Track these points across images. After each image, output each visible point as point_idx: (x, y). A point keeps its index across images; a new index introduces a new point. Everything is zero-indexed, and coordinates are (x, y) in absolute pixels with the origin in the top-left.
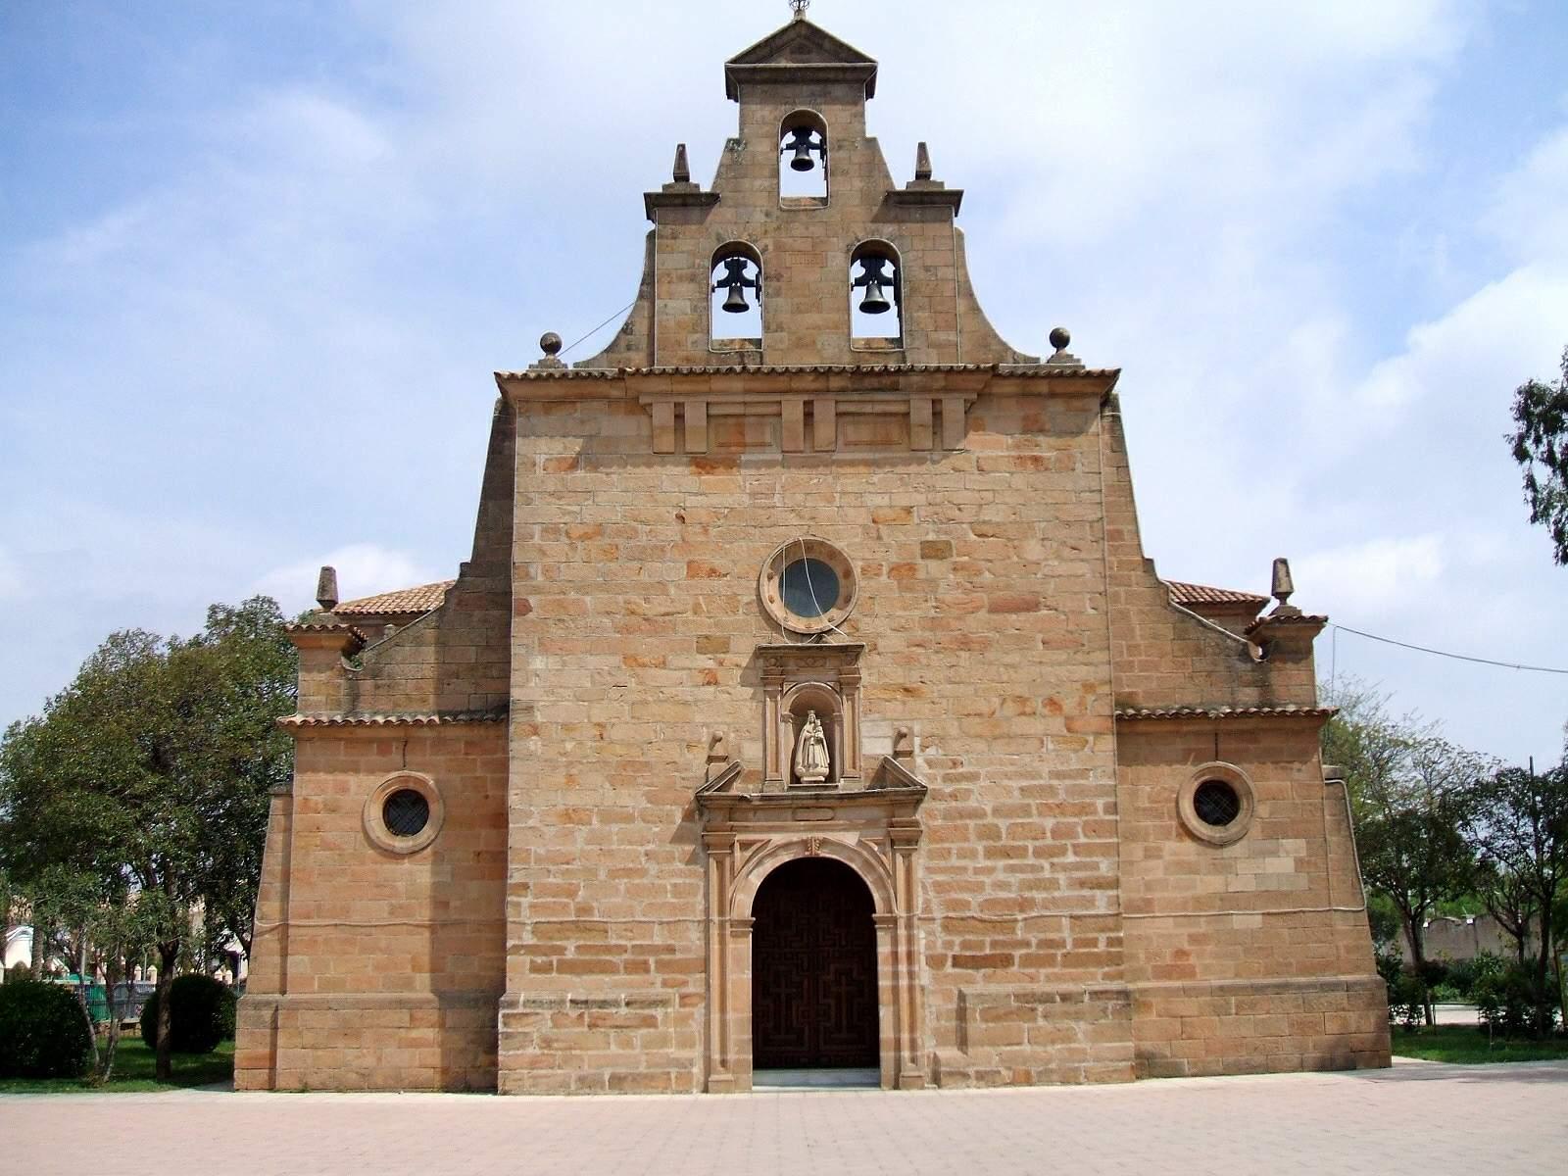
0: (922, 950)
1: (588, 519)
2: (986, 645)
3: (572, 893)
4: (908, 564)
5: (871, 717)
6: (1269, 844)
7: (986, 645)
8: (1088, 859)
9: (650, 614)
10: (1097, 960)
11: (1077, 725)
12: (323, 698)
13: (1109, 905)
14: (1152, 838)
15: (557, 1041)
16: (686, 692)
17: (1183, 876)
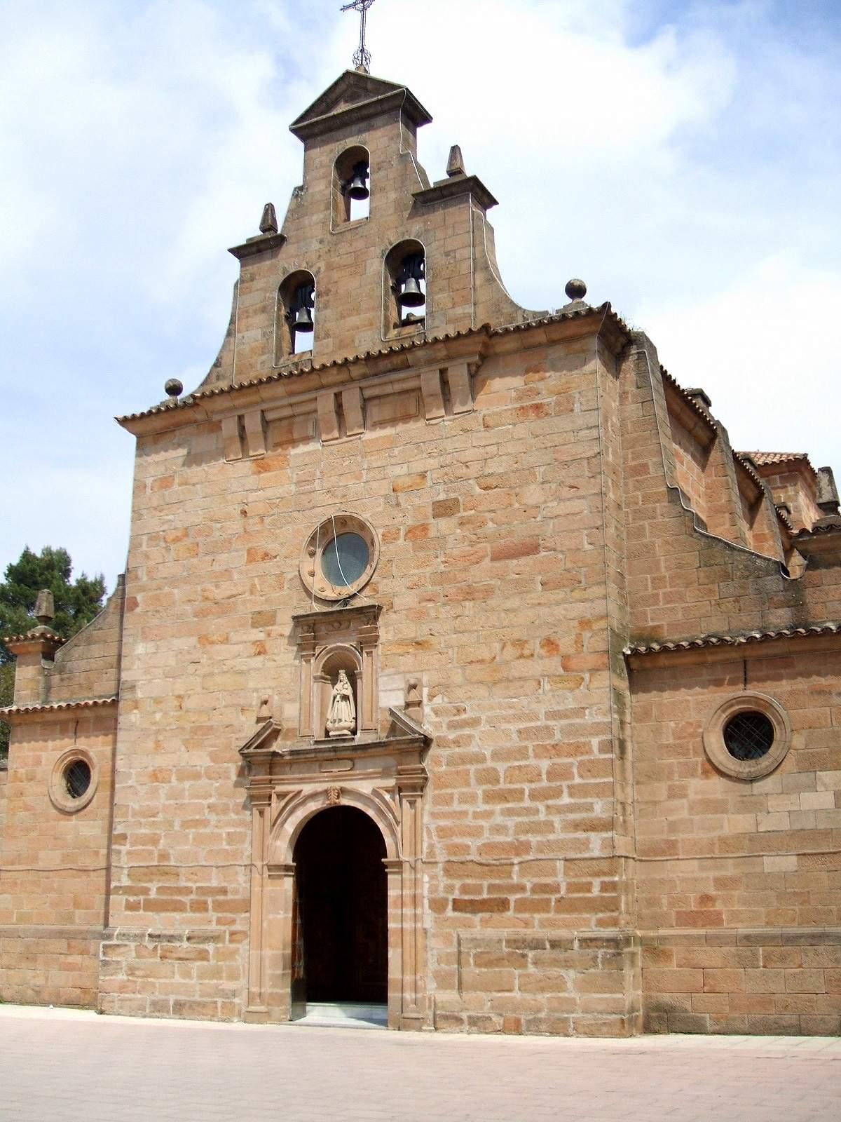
0: (426, 893)
1: (179, 525)
2: (489, 592)
3: (154, 840)
4: (422, 525)
5: (387, 671)
6: (804, 778)
7: (489, 592)
8: (583, 800)
9: (218, 597)
10: (592, 905)
11: (573, 663)
12: (29, 692)
13: (603, 847)
14: (676, 777)
15: (138, 969)
16: (240, 664)
17: (710, 816)
